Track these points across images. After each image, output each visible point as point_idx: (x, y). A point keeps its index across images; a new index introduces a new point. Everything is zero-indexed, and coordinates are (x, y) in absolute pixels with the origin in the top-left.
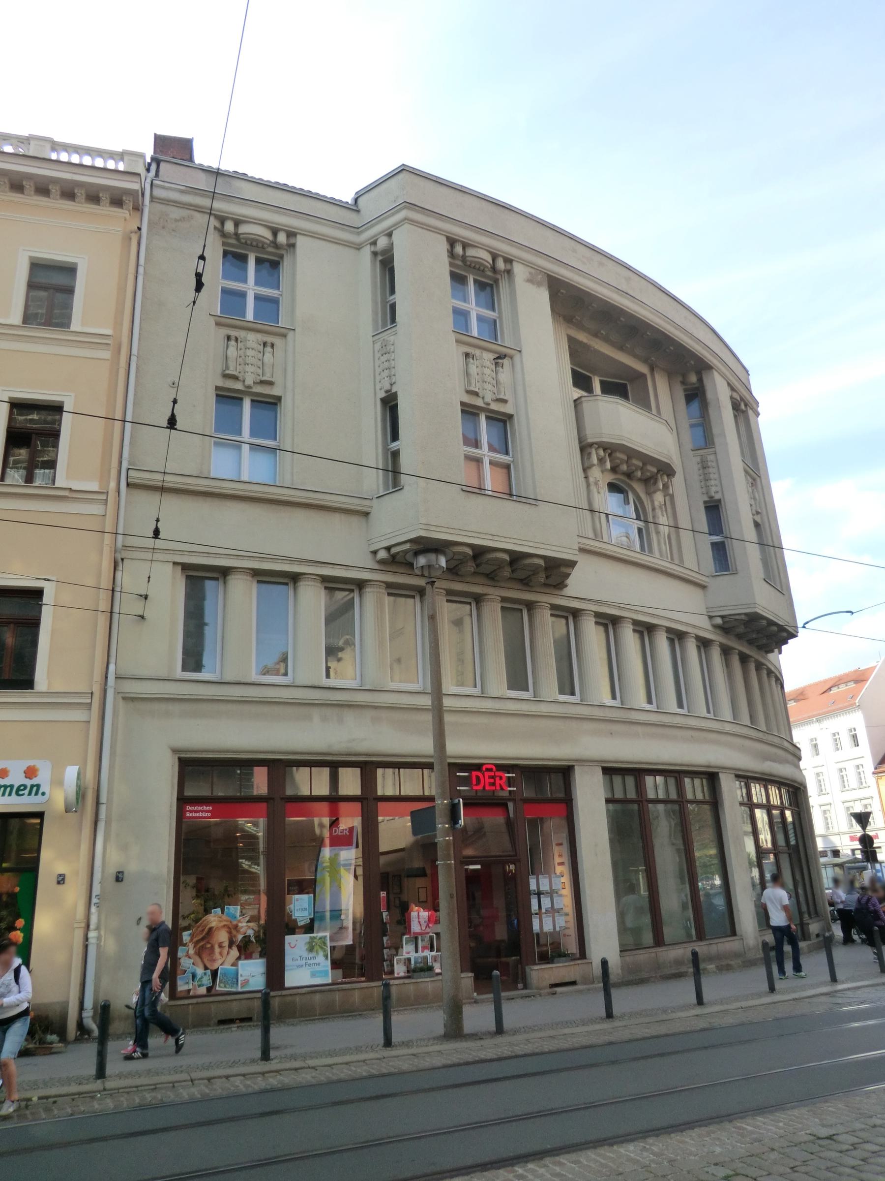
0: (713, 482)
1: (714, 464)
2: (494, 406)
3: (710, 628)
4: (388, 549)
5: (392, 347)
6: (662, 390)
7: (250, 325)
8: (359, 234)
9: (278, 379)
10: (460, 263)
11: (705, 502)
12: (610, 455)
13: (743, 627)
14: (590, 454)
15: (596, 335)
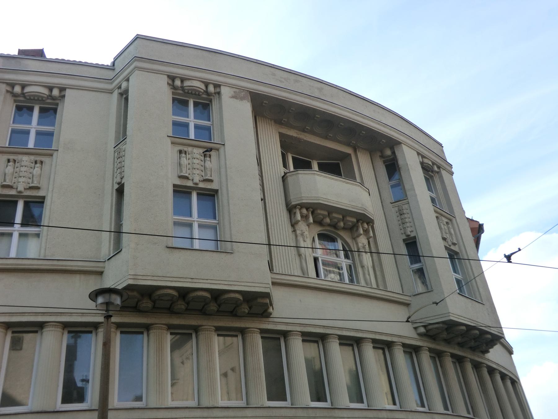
0: (408, 225)
1: (408, 211)
2: (201, 185)
3: (416, 336)
4: (425, 327)
5: (124, 153)
6: (364, 164)
7: (32, 151)
8: (112, 83)
9: (43, 184)
10: (181, 92)
11: (404, 240)
12: (313, 213)
13: (445, 333)
14: (295, 213)
15: (304, 130)
